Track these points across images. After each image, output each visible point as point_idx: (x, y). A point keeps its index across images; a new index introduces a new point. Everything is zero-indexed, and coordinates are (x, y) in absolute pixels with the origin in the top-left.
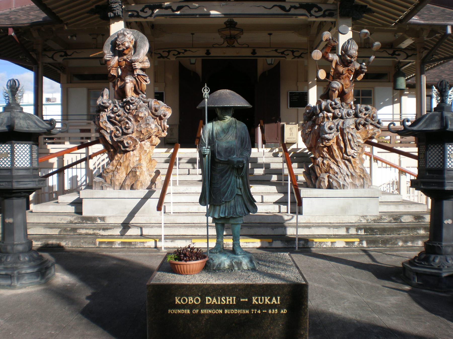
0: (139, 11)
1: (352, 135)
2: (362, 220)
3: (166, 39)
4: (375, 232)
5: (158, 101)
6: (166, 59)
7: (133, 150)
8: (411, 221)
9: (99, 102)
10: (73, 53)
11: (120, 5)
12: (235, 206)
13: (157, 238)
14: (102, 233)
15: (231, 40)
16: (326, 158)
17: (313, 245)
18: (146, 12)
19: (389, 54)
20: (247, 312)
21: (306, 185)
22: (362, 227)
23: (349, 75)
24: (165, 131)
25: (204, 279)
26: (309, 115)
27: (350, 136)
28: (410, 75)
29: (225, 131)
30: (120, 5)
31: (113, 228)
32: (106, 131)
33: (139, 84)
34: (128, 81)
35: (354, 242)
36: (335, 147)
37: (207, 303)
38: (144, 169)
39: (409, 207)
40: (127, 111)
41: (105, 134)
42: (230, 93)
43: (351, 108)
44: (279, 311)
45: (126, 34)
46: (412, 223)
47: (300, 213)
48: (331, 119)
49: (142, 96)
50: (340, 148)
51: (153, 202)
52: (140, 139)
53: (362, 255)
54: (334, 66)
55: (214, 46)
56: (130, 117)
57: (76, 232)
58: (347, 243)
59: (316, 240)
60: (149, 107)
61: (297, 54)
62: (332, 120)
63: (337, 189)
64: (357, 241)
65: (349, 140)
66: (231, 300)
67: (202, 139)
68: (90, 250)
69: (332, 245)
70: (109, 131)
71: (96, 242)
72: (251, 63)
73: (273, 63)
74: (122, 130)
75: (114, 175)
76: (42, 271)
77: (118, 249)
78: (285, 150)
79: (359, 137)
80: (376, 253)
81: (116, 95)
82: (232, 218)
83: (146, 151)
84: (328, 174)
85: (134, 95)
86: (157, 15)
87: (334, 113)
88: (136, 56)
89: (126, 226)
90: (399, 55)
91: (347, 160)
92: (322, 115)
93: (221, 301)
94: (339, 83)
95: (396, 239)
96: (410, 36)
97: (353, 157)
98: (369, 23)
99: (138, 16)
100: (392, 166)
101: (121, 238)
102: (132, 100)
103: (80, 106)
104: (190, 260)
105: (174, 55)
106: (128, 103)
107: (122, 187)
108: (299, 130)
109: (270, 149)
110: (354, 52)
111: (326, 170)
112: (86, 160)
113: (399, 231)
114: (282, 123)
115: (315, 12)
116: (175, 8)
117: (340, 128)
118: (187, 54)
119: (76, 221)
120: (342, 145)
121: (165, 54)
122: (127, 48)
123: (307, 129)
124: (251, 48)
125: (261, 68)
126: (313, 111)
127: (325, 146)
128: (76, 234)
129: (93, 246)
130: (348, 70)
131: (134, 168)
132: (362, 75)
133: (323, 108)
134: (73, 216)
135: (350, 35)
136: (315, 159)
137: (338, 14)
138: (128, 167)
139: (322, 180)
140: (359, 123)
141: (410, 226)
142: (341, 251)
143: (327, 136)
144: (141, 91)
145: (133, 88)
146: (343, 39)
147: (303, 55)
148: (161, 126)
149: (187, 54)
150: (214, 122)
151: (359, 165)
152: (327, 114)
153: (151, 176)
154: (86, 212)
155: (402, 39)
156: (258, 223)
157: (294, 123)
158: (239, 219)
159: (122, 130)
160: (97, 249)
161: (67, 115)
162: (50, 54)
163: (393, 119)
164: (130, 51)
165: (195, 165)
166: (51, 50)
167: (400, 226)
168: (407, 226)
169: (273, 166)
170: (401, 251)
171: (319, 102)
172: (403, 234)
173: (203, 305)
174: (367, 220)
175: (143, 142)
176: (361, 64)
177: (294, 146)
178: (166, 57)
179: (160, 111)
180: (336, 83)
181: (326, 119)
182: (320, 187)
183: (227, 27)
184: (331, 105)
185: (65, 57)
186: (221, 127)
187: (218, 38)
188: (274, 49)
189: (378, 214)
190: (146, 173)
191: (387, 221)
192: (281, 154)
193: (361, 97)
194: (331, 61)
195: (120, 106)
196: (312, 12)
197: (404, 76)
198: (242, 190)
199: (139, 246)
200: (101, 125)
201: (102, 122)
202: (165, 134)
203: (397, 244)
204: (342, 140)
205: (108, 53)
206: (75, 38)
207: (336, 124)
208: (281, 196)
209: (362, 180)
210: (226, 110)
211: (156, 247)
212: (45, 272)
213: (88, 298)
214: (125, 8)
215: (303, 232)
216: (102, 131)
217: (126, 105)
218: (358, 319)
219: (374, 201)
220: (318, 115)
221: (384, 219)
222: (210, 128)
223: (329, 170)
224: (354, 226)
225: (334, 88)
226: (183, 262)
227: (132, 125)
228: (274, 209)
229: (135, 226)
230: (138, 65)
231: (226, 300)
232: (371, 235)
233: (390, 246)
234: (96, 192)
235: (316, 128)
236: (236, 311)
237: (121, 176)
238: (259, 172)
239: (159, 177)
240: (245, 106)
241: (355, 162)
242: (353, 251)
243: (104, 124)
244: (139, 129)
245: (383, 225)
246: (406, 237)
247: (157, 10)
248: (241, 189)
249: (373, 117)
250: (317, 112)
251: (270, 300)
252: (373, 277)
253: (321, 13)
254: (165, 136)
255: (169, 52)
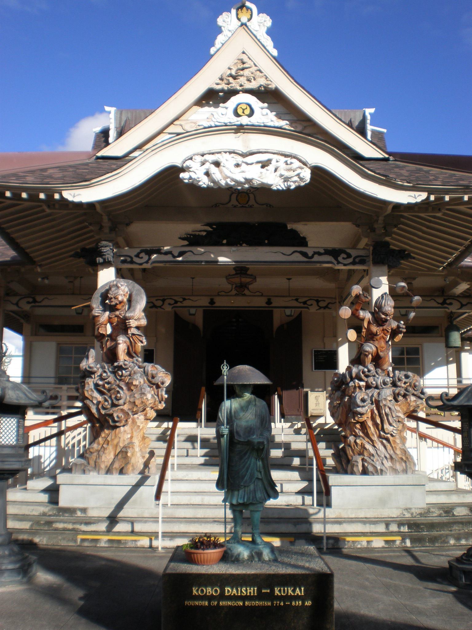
0: (133, 256)
1: (390, 408)
2: (406, 514)
3: (161, 283)
4: (422, 529)
5: (156, 366)
6: (159, 310)
7: (124, 426)
8: (465, 514)
9: (84, 365)
10: (43, 300)
11: (111, 249)
12: (255, 491)
13: (153, 535)
14: (84, 528)
15: (241, 288)
16: (360, 436)
17: (345, 545)
18: (142, 258)
19: (438, 303)
20: (269, 604)
21: (335, 471)
22: (405, 522)
23: (385, 336)
24: (163, 402)
25: (223, 569)
26: (338, 384)
27: (387, 410)
28: (467, 328)
29: (244, 408)
30: (111, 249)
31: (98, 523)
32: (92, 401)
33: (133, 345)
34: (120, 342)
35: (394, 541)
36: (370, 423)
37: (226, 594)
38: (137, 449)
39: (464, 497)
40: (118, 377)
41: (91, 405)
42: (250, 370)
43: (388, 375)
44: (303, 603)
45: (120, 286)
46: (467, 517)
47: (329, 505)
48: (363, 389)
49: (137, 360)
50: (375, 424)
51: (147, 491)
52: (133, 412)
53: (403, 556)
54: (366, 324)
55: (220, 294)
56: (122, 384)
57: (51, 526)
58: (387, 542)
59: (348, 539)
60: (145, 373)
61: (322, 304)
62: (365, 390)
63: (373, 474)
64: (398, 539)
65: (387, 415)
66: (252, 591)
67: (219, 418)
68: (69, 548)
69: (367, 545)
70: (95, 402)
71: (77, 539)
72: (265, 315)
73: (292, 314)
74: (112, 401)
75: (99, 456)
76: (24, 570)
77: (104, 549)
78: (309, 426)
79: (399, 410)
80: (422, 553)
81: (105, 358)
82: (252, 504)
83: (139, 426)
84: (362, 457)
85: (127, 358)
86: (154, 262)
87: (367, 382)
88: (131, 312)
89: (113, 519)
90: (451, 304)
91: (385, 439)
92: (353, 384)
93: (241, 592)
94: (373, 346)
95: (447, 536)
96: (464, 280)
97: (392, 435)
98: (411, 266)
99: (132, 262)
100: (445, 445)
101: (108, 535)
102: (125, 365)
103: (47, 365)
104: (207, 549)
105: (170, 304)
106: (120, 368)
107: (109, 471)
108: (327, 399)
109: (290, 424)
110: (390, 309)
111: (360, 451)
112: (60, 434)
113: (451, 527)
114: (305, 390)
115: (344, 258)
116: (176, 254)
117: (376, 400)
118: (186, 303)
119: (51, 513)
120: (379, 421)
121: (159, 303)
122: (121, 302)
123: (336, 400)
124: (265, 296)
125: (278, 319)
126: (342, 380)
127: (358, 422)
128: (51, 529)
129: (73, 544)
130: (383, 330)
131: (125, 447)
132: (401, 336)
133: (354, 375)
134: (47, 506)
135: (385, 288)
136: (346, 437)
137: (371, 262)
138: (117, 446)
139: (355, 463)
140: (399, 394)
141: (464, 520)
142: (378, 552)
143: (359, 409)
144: (135, 353)
145: (126, 351)
146: (376, 294)
147: (330, 306)
148: (158, 395)
149: (187, 303)
150: (232, 400)
151: (400, 445)
152: (358, 383)
153: (144, 457)
154: (64, 500)
155: (457, 284)
156: (278, 518)
157: (320, 390)
158: (259, 505)
159: (112, 401)
160: (78, 548)
161: (29, 377)
162: (15, 299)
163: (448, 384)
164: (123, 306)
165: (196, 444)
166: (16, 294)
167: (451, 521)
168: (460, 520)
169: (294, 446)
170: (453, 550)
171: (349, 369)
172: (455, 530)
173: (222, 596)
174: (412, 514)
175: (136, 416)
176: (399, 322)
177: (321, 421)
178: (160, 307)
179: (157, 378)
180: (369, 346)
181: (358, 390)
182: (353, 473)
183: (236, 274)
184: (363, 372)
185: (33, 304)
186: (240, 404)
187: (222, 283)
188: (294, 298)
189: (425, 506)
190: (139, 454)
191: (436, 515)
192: (304, 431)
193: (405, 356)
194: (363, 320)
195: (110, 372)
196: (340, 259)
197: (458, 329)
198: (262, 473)
199: (130, 545)
200: (86, 394)
201: (88, 391)
202: (162, 406)
203: (448, 542)
204: (377, 414)
205: (97, 310)
206: (46, 281)
207: (370, 395)
208: (304, 484)
209: (404, 464)
210: (245, 387)
211: (151, 547)
212: (27, 569)
213: (81, 599)
214: (116, 252)
215: (332, 529)
216: (88, 402)
217: (118, 370)
218: (393, 620)
219: (419, 490)
220: (348, 384)
221: (432, 512)
222: (228, 405)
223: (363, 451)
224: (395, 521)
225: (367, 352)
226: (200, 551)
227: (124, 394)
228: (297, 500)
229: (125, 520)
230: (133, 323)
231: (246, 590)
232: (417, 532)
233: (439, 545)
234: (77, 477)
235: (346, 400)
236: (257, 603)
237: (108, 457)
238: (276, 453)
239: (153, 460)
240: (266, 383)
241: (394, 441)
242: (394, 551)
243: (90, 393)
244: (132, 400)
245: (431, 520)
246: (459, 534)
247: (155, 255)
248: (261, 472)
249: (415, 386)
250: (346, 381)
251: (294, 591)
252: (415, 579)
253: (351, 260)
254: (162, 408)
255: (164, 301)
